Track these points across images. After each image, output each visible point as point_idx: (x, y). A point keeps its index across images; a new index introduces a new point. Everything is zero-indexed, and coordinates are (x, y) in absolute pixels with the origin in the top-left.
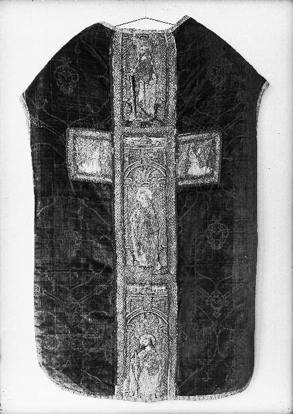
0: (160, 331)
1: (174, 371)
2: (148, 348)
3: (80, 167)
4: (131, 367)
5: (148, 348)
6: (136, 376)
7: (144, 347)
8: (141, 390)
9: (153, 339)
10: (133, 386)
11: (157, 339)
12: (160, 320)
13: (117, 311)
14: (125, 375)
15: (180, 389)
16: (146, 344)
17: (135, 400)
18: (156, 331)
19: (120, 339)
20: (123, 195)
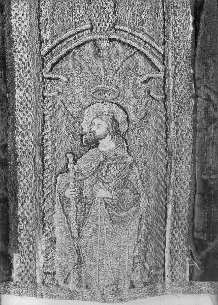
0: (141, 92)
1: (184, 212)
2: (107, 144)
3: (129, 178)
4: (57, 200)
5: (107, 144)
6: (74, 227)
7: (95, 143)
8: (89, 270)
9: (120, 117)
10: (62, 260)
11: (132, 117)
12: (141, 59)
13: (14, 35)
14: (42, 224)
15: (205, 262)
16: (100, 132)
17: (71, 295)
18: (129, 93)
19: (24, 116)
20: (196, 187)
